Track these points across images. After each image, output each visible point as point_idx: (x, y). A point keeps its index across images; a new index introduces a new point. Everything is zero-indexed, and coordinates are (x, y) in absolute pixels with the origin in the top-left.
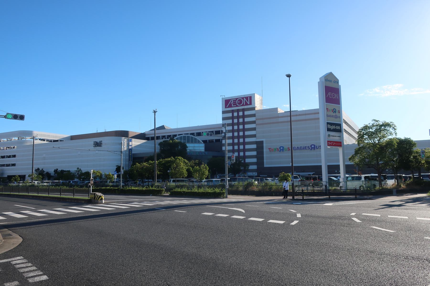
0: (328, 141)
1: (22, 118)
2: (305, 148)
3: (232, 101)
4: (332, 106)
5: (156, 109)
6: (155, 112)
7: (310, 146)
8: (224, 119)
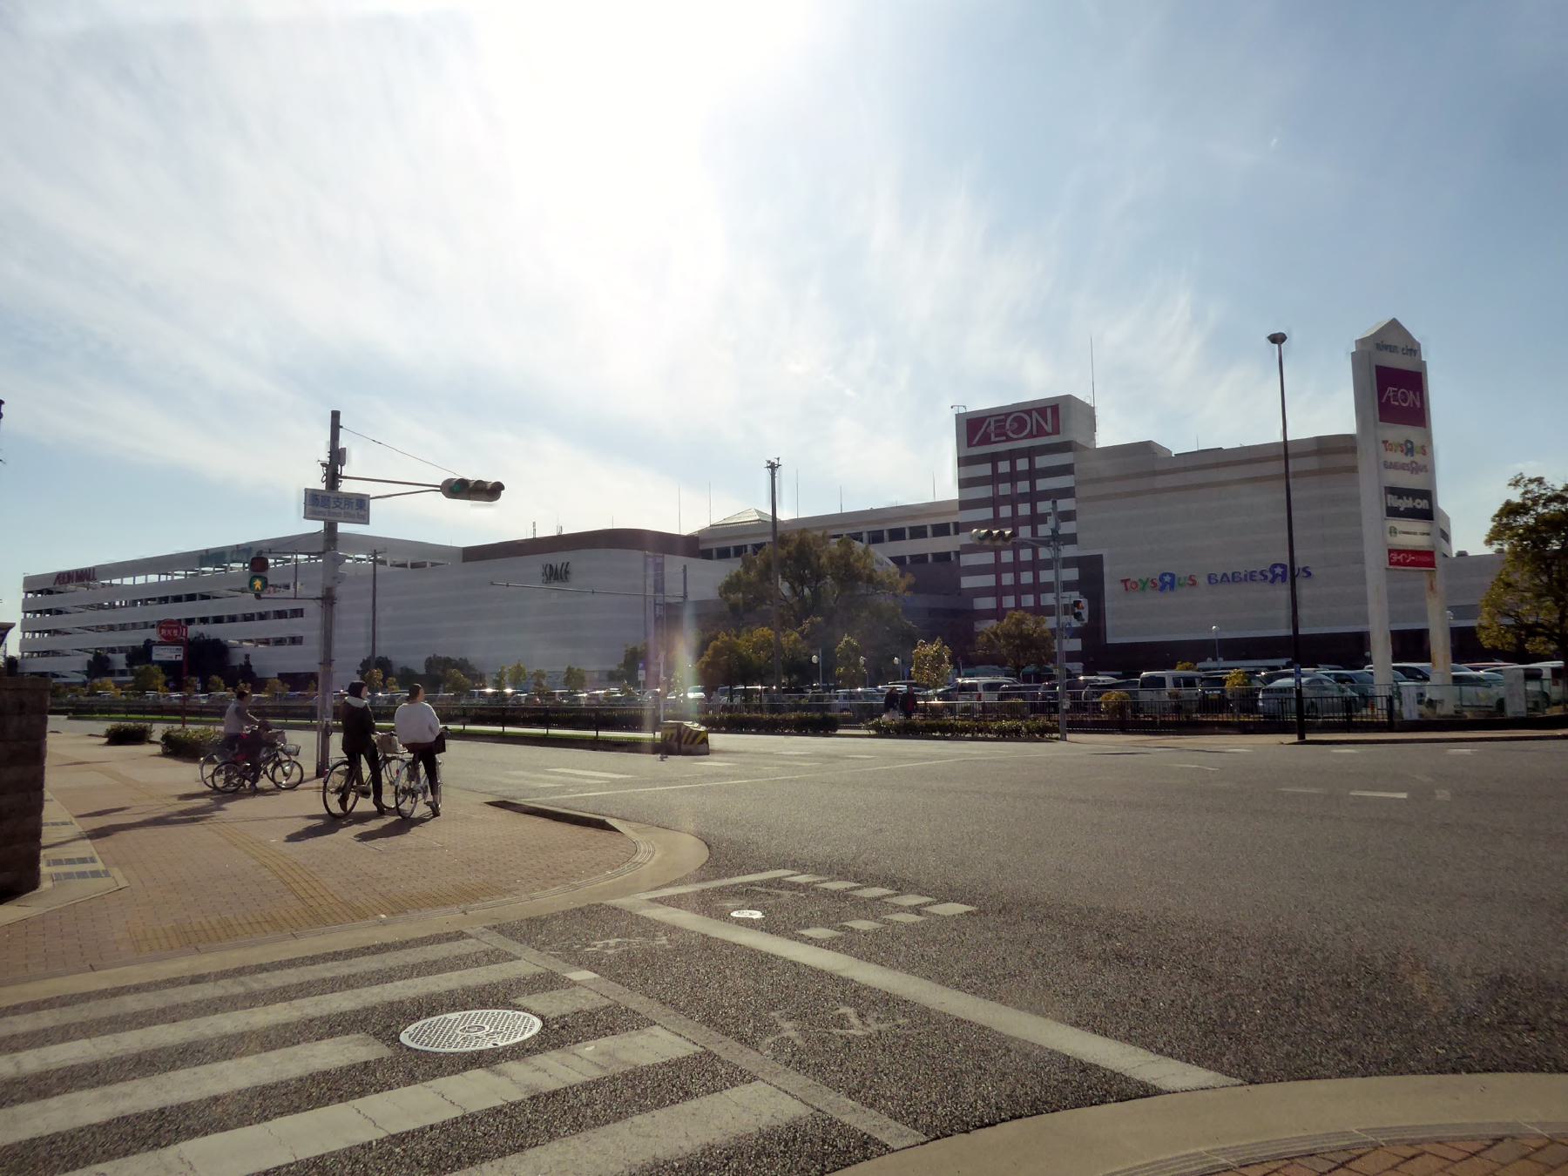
0: (1390, 551)
1: (490, 492)
2: (1251, 577)
3: (990, 422)
4: (1399, 433)
5: (778, 459)
6: (773, 467)
7: (1267, 568)
8: (964, 483)
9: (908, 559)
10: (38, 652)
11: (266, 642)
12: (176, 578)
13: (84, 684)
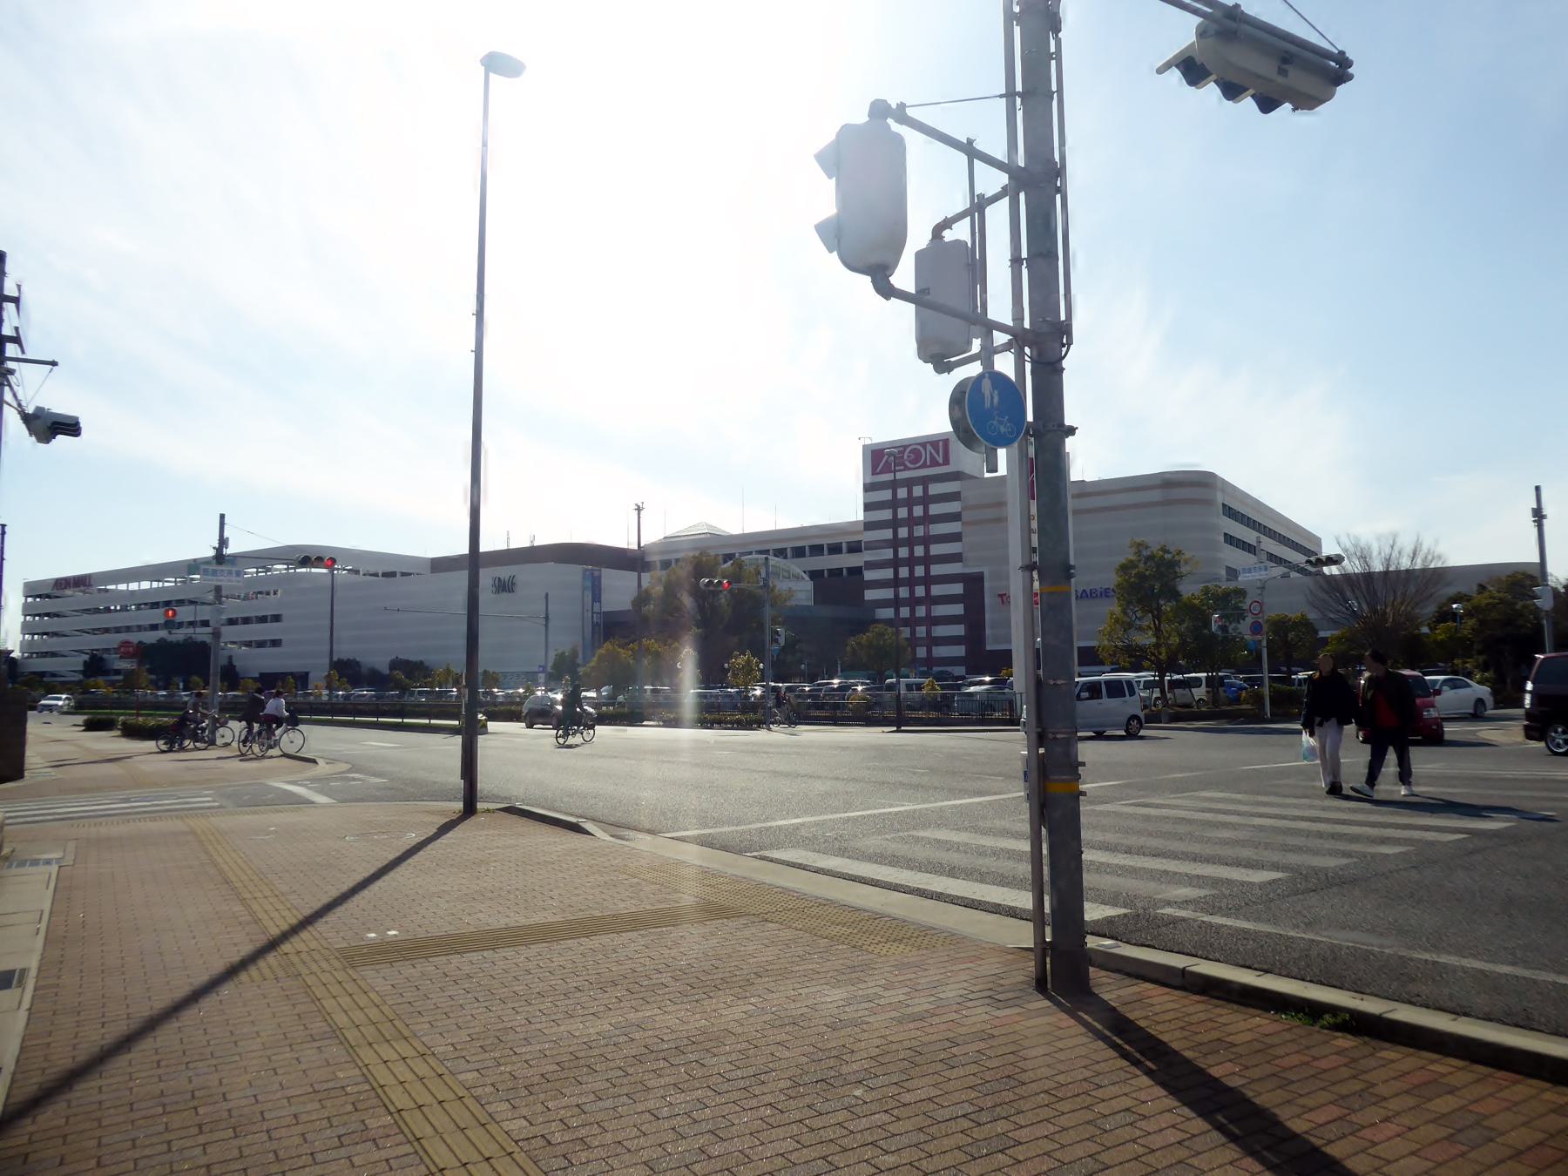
6: (639, 509)
8: (868, 507)
9: (845, 571)
10: (37, 653)
11: (248, 644)
12: (166, 584)
13: (79, 683)
